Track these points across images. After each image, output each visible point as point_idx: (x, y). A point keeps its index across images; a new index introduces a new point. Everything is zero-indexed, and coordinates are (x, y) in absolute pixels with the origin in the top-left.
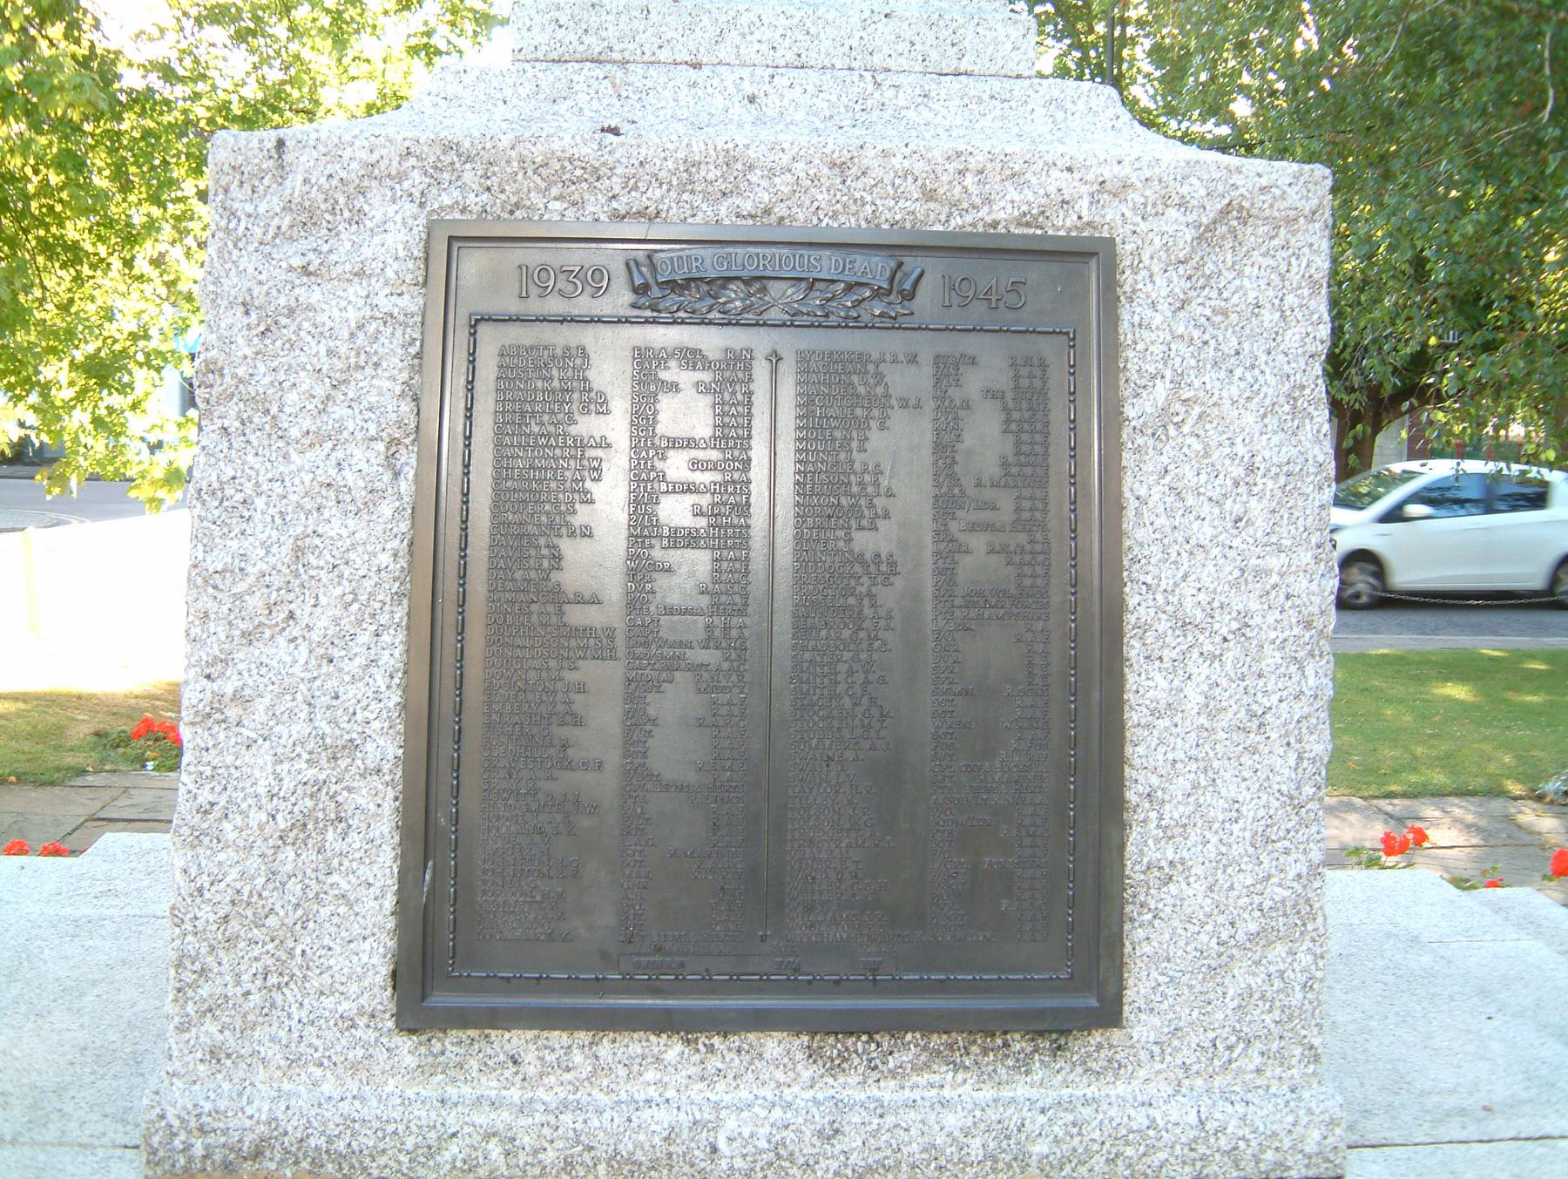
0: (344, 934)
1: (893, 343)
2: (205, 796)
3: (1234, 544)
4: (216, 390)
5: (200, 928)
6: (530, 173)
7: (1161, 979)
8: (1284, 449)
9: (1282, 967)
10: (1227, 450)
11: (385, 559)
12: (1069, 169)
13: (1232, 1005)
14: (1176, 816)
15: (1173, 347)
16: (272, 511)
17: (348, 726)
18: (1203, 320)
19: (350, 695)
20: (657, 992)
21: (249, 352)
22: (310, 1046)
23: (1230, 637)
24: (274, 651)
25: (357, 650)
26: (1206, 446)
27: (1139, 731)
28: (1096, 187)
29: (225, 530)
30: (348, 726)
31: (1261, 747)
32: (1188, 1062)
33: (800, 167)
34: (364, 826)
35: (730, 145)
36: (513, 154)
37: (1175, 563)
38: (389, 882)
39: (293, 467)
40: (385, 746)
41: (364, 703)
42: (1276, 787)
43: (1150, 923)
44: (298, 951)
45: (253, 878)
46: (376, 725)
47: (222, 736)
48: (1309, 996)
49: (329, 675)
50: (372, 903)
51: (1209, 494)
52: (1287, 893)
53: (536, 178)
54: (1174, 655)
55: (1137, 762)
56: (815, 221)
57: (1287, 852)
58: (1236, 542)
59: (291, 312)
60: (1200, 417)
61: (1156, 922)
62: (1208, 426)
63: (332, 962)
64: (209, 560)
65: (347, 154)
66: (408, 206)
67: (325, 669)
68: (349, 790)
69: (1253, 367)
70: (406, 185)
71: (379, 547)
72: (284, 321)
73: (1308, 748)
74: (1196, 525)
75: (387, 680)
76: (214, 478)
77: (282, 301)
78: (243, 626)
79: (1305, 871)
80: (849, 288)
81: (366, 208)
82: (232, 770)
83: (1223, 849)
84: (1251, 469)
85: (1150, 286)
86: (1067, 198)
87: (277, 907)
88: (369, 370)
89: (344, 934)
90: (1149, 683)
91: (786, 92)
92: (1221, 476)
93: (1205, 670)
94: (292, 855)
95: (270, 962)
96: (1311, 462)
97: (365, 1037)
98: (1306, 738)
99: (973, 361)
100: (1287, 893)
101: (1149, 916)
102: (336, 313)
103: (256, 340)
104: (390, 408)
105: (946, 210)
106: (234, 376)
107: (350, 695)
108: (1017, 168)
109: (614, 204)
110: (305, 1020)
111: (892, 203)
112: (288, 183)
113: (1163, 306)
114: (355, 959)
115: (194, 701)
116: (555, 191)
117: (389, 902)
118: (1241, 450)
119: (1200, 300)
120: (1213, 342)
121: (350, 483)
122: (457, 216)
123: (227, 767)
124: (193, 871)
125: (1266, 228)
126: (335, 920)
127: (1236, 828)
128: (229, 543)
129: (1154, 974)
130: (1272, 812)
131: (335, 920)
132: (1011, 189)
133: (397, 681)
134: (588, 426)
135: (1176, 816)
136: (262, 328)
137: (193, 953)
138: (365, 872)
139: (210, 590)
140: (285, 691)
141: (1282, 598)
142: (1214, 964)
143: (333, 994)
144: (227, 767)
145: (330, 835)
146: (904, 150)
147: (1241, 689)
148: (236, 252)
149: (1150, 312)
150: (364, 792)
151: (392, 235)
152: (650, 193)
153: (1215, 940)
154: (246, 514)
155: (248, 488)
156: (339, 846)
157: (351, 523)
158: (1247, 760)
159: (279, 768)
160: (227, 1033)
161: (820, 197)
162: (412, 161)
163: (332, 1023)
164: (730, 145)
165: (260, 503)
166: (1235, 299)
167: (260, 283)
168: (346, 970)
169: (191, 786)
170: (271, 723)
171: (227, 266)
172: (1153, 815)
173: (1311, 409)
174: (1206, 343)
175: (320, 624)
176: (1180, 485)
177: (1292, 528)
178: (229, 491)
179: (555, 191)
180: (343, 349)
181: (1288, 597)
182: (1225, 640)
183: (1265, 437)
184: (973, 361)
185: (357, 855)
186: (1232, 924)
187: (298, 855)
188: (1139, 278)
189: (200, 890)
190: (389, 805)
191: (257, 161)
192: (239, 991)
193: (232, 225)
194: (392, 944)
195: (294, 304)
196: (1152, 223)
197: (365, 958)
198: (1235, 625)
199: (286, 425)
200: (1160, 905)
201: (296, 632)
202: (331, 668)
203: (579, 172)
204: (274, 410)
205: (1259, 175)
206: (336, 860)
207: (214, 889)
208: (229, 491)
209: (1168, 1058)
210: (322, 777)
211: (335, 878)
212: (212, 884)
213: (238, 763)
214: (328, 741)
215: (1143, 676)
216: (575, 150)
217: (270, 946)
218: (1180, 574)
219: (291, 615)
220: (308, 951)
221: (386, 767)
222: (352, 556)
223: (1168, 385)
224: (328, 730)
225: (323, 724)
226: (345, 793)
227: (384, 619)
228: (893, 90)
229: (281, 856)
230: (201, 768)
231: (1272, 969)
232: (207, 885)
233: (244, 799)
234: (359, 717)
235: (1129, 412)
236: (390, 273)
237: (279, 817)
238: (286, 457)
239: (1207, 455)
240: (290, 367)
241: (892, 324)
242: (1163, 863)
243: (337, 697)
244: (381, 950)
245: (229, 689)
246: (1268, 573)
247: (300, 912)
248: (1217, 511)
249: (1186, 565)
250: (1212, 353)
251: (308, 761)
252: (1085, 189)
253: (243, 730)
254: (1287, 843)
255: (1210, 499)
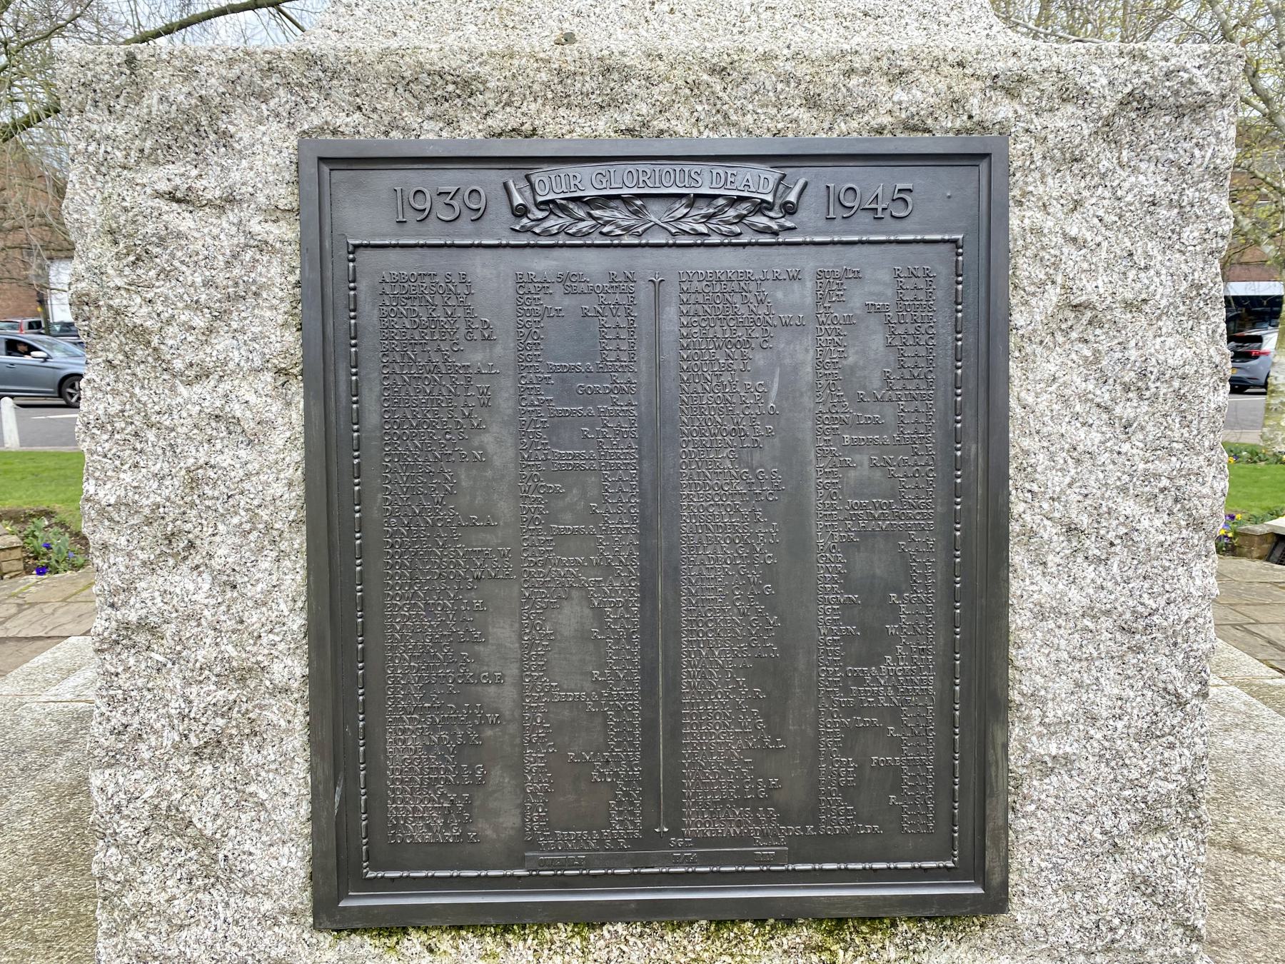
0: (264, 838)
1: (779, 260)
2: (118, 718)
3: (1123, 450)
4: (95, 322)
5: (120, 842)
6: (401, 90)
7: (1043, 865)
8: (1179, 352)
9: (1164, 852)
10: (1118, 355)
11: (278, 489)
12: (961, 64)
13: (1115, 889)
14: (1060, 713)
15: (1065, 250)
16: (162, 443)
17: (255, 649)
18: (1096, 221)
19: (254, 620)
20: (664, 668)
21: (119, 282)
22: (234, 944)
23: (1117, 541)
24: (177, 578)
25: (260, 575)
26: (1096, 351)
27: (1023, 635)
28: (989, 82)
29: (118, 463)
30: (255, 649)
31: (1147, 647)
32: (1071, 941)
33: (679, 71)
34: (277, 741)
35: (606, 53)
36: (380, 68)
37: (1061, 470)
38: (304, 791)
39: (179, 400)
40: (291, 668)
41: (269, 626)
42: (1161, 685)
43: (1033, 814)
44: (221, 856)
45: (169, 794)
46: (282, 646)
47: (132, 661)
48: (1192, 881)
49: (234, 600)
50: (289, 812)
51: (1098, 400)
52: (1172, 786)
53: (407, 95)
54: (1058, 560)
55: (1020, 663)
56: (695, 133)
57: (1171, 746)
58: (1126, 447)
59: (162, 241)
60: (1090, 323)
61: (1039, 813)
62: (1098, 331)
63: (252, 867)
64: (101, 494)
65: (203, 70)
66: (275, 126)
67: (229, 594)
68: (261, 707)
69: (1146, 268)
70: (272, 103)
71: (272, 477)
72: (155, 250)
73: (1195, 646)
74: (1082, 433)
75: (291, 603)
76: (101, 412)
77: (150, 228)
78: (143, 556)
79: (1189, 764)
80: (734, 201)
81: (232, 129)
82: (145, 693)
83: (1107, 744)
84: (1143, 375)
85: (1041, 189)
86: (958, 96)
87: (195, 820)
88: (251, 300)
89: (264, 838)
90: (1035, 588)
91: (667, 18)
92: (1111, 381)
93: (1090, 572)
94: (210, 769)
95: (194, 868)
96: (1206, 363)
97: (287, 935)
98: (1192, 638)
99: (857, 276)
100: (1172, 786)
101: (1033, 807)
102: (209, 240)
103: (127, 271)
104: (273, 338)
105: (829, 118)
106: (110, 307)
107: (254, 620)
108: (905, 65)
109: (490, 121)
110: (230, 920)
111: (774, 111)
112: (145, 102)
113: (1055, 208)
114: (274, 863)
115: (100, 630)
116: (429, 110)
117: (305, 809)
118: (1133, 354)
119: (1094, 200)
120: (1105, 244)
121: (238, 414)
122: (329, 137)
123: (140, 690)
124: (110, 790)
125: (1167, 119)
126: (256, 825)
127: (1120, 724)
128: (122, 476)
129: (1037, 860)
130: (1157, 709)
131: (256, 825)
132: (898, 90)
133: (299, 604)
134: (476, 357)
135: (1060, 713)
136: (132, 258)
137: (116, 864)
138: (281, 783)
139: (107, 523)
140: (189, 618)
141: (1170, 502)
142: (1097, 851)
143: (256, 895)
144: (140, 690)
145: (246, 748)
146: (786, 51)
147: (1126, 592)
148: (99, 178)
149: (1040, 215)
150: (275, 709)
151: (263, 158)
152: (524, 109)
153: (1098, 830)
154: (138, 446)
155: (138, 420)
156: (256, 758)
157: (242, 453)
158: (1131, 659)
159: (188, 691)
160: (152, 938)
161: (699, 108)
162: (276, 78)
163: (255, 922)
164: (606, 53)
165: (151, 435)
166: (1129, 198)
167: (126, 210)
168: (266, 874)
169: (103, 709)
170: (178, 648)
171: (91, 193)
172: (1037, 712)
173: (1207, 309)
174: (1099, 245)
175: (220, 552)
176: (1068, 392)
177: (1185, 431)
178: (119, 425)
179: (429, 110)
180: (220, 279)
181: (1176, 501)
182: (1112, 544)
183: (1158, 340)
184: (857, 276)
185: (273, 767)
186: (1115, 814)
187: (217, 768)
188: (1030, 179)
189: (118, 808)
190: (300, 721)
191: (107, 77)
192: (164, 896)
193: (91, 149)
194: (309, 847)
195: (163, 233)
196: (1046, 119)
197: (284, 863)
198: (1122, 530)
199: (169, 357)
200: (1043, 797)
201: (198, 560)
202: (235, 594)
203: (451, 88)
204: (155, 341)
205: (1166, 59)
206: (252, 772)
207: (131, 806)
208: (119, 425)
209: (1052, 939)
210: (232, 698)
211: (252, 788)
212: (129, 801)
213: (150, 686)
214: (235, 664)
215: (1028, 582)
216: (445, 63)
217: (193, 854)
218: (1068, 480)
219: (191, 545)
220: (231, 857)
221: (295, 685)
222: (247, 485)
223: (1058, 290)
224: (234, 654)
225: (230, 648)
226: (257, 711)
227: (284, 545)
228: (769, 13)
229: (199, 771)
230: (111, 692)
231: (1155, 855)
232: (124, 803)
233: (158, 719)
234: (264, 641)
235: (1018, 319)
236: (261, 198)
237: (192, 736)
238: (173, 389)
239: (1097, 360)
240: (167, 298)
241: (774, 240)
242: (1047, 758)
243: (242, 622)
244: (299, 854)
245: (133, 617)
246: (1158, 476)
247: (219, 822)
248: (1105, 416)
249: (1073, 472)
250: (1104, 255)
251: (216, 683)
252: (977, 85)
253: (153, 654)
254: (1171, 739)
255: (1098, 405)
